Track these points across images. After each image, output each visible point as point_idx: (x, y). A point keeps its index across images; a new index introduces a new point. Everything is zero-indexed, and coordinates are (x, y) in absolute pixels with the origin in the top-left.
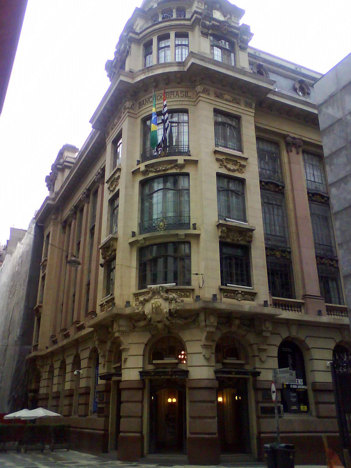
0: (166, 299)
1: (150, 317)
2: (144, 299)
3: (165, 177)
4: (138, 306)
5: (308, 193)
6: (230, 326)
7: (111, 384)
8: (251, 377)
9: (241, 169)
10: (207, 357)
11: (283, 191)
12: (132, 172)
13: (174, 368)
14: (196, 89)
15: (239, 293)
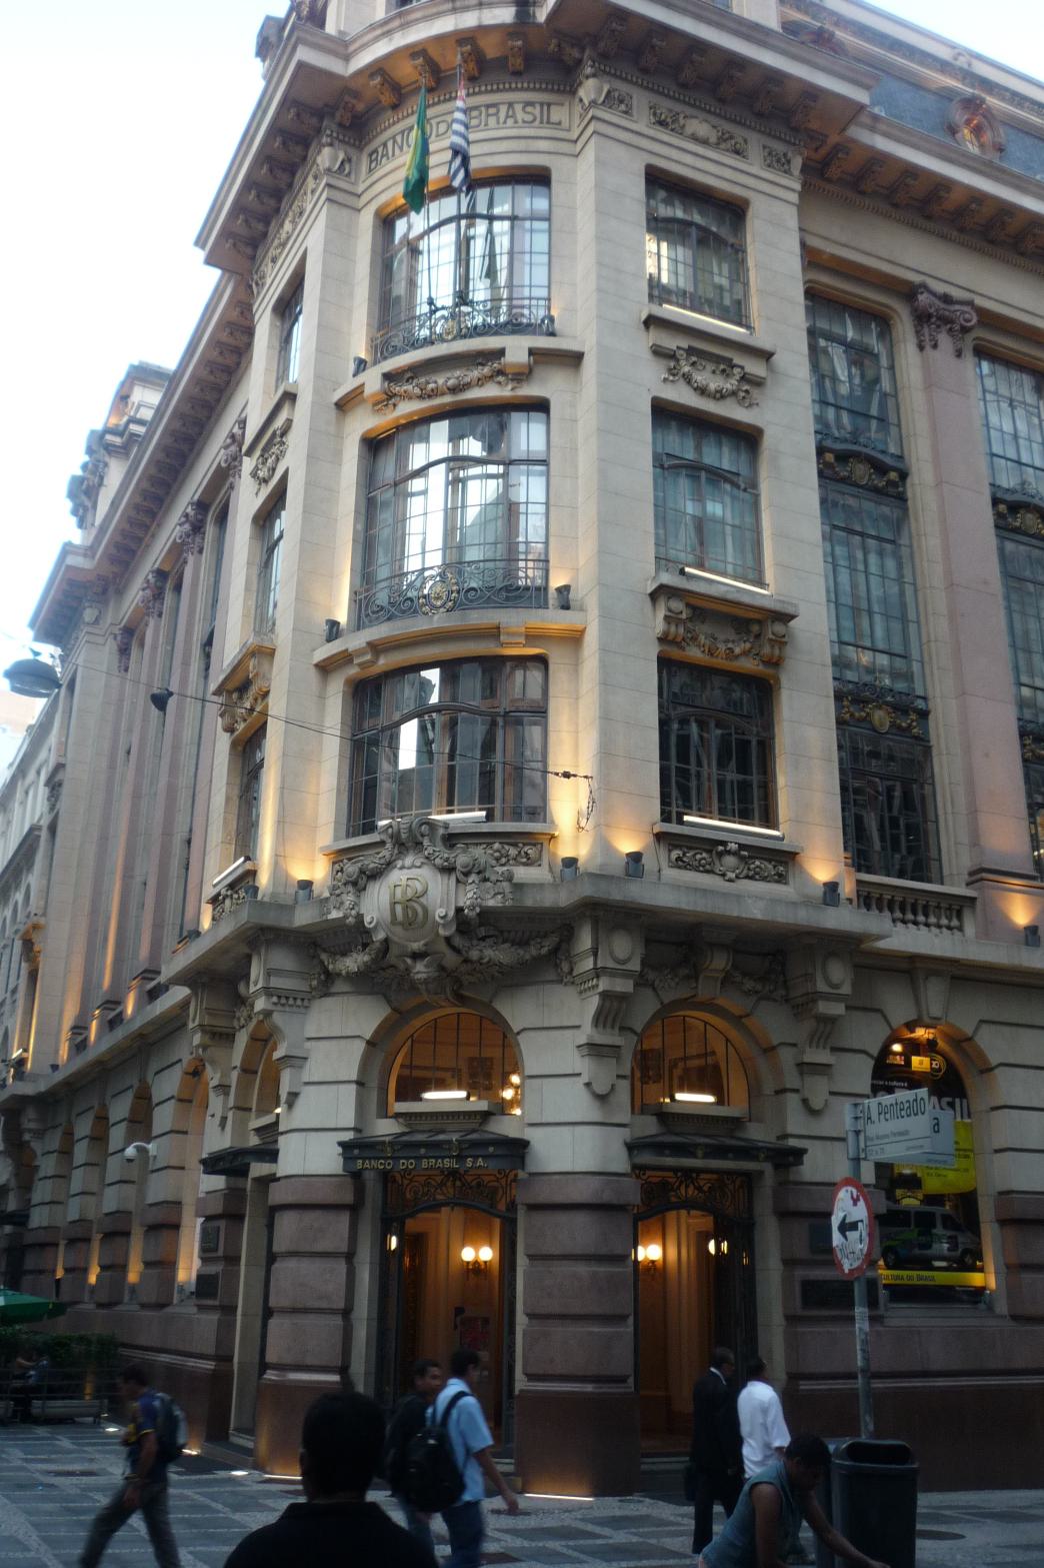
0: (448, 870)
1: (380, 936)
2: (362, 872)
3: (462, 414)
4: (338, 895)
5: (995, 502)
6: (694, 976)
7: (245, 1190)
8: (768, 1168)
9: (747, 391)
10: (601, 1089)
11: (901, 489)
12: (336, 404)
13: (474, 1131)
14: (581, 93)
15: (729, 852)
